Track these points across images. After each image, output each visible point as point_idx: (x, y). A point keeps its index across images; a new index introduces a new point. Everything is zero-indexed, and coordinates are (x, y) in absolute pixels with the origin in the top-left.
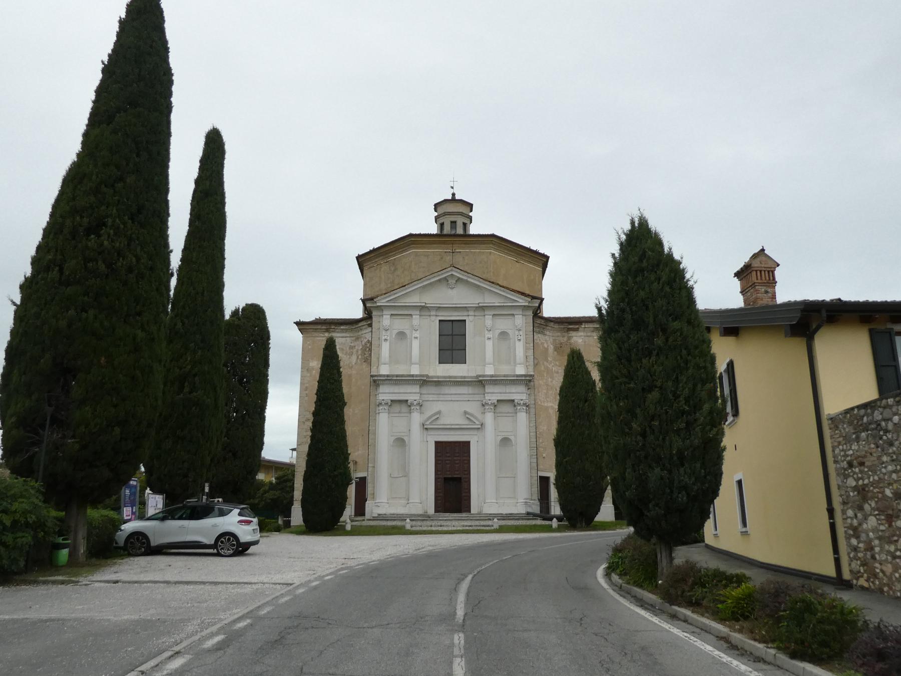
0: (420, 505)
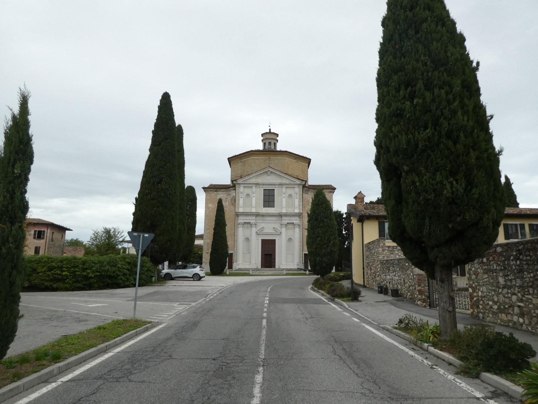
0: (255, 265)
